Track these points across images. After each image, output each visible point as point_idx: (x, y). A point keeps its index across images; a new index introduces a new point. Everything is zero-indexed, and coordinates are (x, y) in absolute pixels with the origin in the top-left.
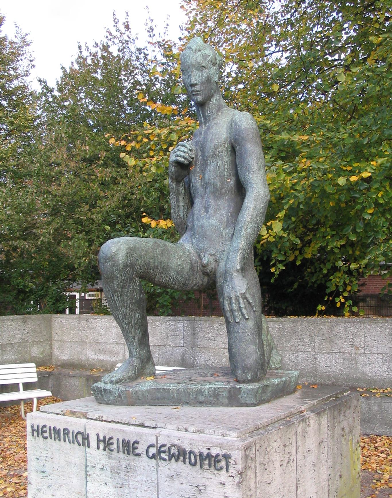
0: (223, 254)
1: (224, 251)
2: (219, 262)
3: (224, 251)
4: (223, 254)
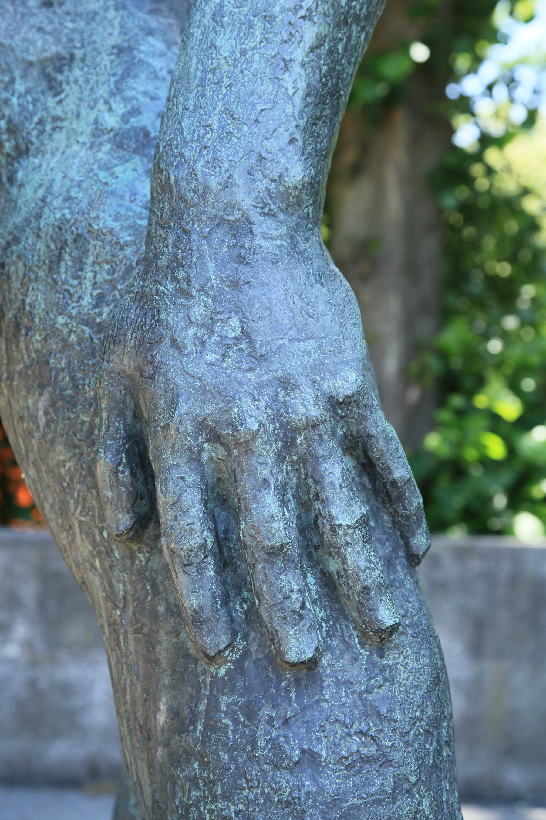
0: (54, 87)
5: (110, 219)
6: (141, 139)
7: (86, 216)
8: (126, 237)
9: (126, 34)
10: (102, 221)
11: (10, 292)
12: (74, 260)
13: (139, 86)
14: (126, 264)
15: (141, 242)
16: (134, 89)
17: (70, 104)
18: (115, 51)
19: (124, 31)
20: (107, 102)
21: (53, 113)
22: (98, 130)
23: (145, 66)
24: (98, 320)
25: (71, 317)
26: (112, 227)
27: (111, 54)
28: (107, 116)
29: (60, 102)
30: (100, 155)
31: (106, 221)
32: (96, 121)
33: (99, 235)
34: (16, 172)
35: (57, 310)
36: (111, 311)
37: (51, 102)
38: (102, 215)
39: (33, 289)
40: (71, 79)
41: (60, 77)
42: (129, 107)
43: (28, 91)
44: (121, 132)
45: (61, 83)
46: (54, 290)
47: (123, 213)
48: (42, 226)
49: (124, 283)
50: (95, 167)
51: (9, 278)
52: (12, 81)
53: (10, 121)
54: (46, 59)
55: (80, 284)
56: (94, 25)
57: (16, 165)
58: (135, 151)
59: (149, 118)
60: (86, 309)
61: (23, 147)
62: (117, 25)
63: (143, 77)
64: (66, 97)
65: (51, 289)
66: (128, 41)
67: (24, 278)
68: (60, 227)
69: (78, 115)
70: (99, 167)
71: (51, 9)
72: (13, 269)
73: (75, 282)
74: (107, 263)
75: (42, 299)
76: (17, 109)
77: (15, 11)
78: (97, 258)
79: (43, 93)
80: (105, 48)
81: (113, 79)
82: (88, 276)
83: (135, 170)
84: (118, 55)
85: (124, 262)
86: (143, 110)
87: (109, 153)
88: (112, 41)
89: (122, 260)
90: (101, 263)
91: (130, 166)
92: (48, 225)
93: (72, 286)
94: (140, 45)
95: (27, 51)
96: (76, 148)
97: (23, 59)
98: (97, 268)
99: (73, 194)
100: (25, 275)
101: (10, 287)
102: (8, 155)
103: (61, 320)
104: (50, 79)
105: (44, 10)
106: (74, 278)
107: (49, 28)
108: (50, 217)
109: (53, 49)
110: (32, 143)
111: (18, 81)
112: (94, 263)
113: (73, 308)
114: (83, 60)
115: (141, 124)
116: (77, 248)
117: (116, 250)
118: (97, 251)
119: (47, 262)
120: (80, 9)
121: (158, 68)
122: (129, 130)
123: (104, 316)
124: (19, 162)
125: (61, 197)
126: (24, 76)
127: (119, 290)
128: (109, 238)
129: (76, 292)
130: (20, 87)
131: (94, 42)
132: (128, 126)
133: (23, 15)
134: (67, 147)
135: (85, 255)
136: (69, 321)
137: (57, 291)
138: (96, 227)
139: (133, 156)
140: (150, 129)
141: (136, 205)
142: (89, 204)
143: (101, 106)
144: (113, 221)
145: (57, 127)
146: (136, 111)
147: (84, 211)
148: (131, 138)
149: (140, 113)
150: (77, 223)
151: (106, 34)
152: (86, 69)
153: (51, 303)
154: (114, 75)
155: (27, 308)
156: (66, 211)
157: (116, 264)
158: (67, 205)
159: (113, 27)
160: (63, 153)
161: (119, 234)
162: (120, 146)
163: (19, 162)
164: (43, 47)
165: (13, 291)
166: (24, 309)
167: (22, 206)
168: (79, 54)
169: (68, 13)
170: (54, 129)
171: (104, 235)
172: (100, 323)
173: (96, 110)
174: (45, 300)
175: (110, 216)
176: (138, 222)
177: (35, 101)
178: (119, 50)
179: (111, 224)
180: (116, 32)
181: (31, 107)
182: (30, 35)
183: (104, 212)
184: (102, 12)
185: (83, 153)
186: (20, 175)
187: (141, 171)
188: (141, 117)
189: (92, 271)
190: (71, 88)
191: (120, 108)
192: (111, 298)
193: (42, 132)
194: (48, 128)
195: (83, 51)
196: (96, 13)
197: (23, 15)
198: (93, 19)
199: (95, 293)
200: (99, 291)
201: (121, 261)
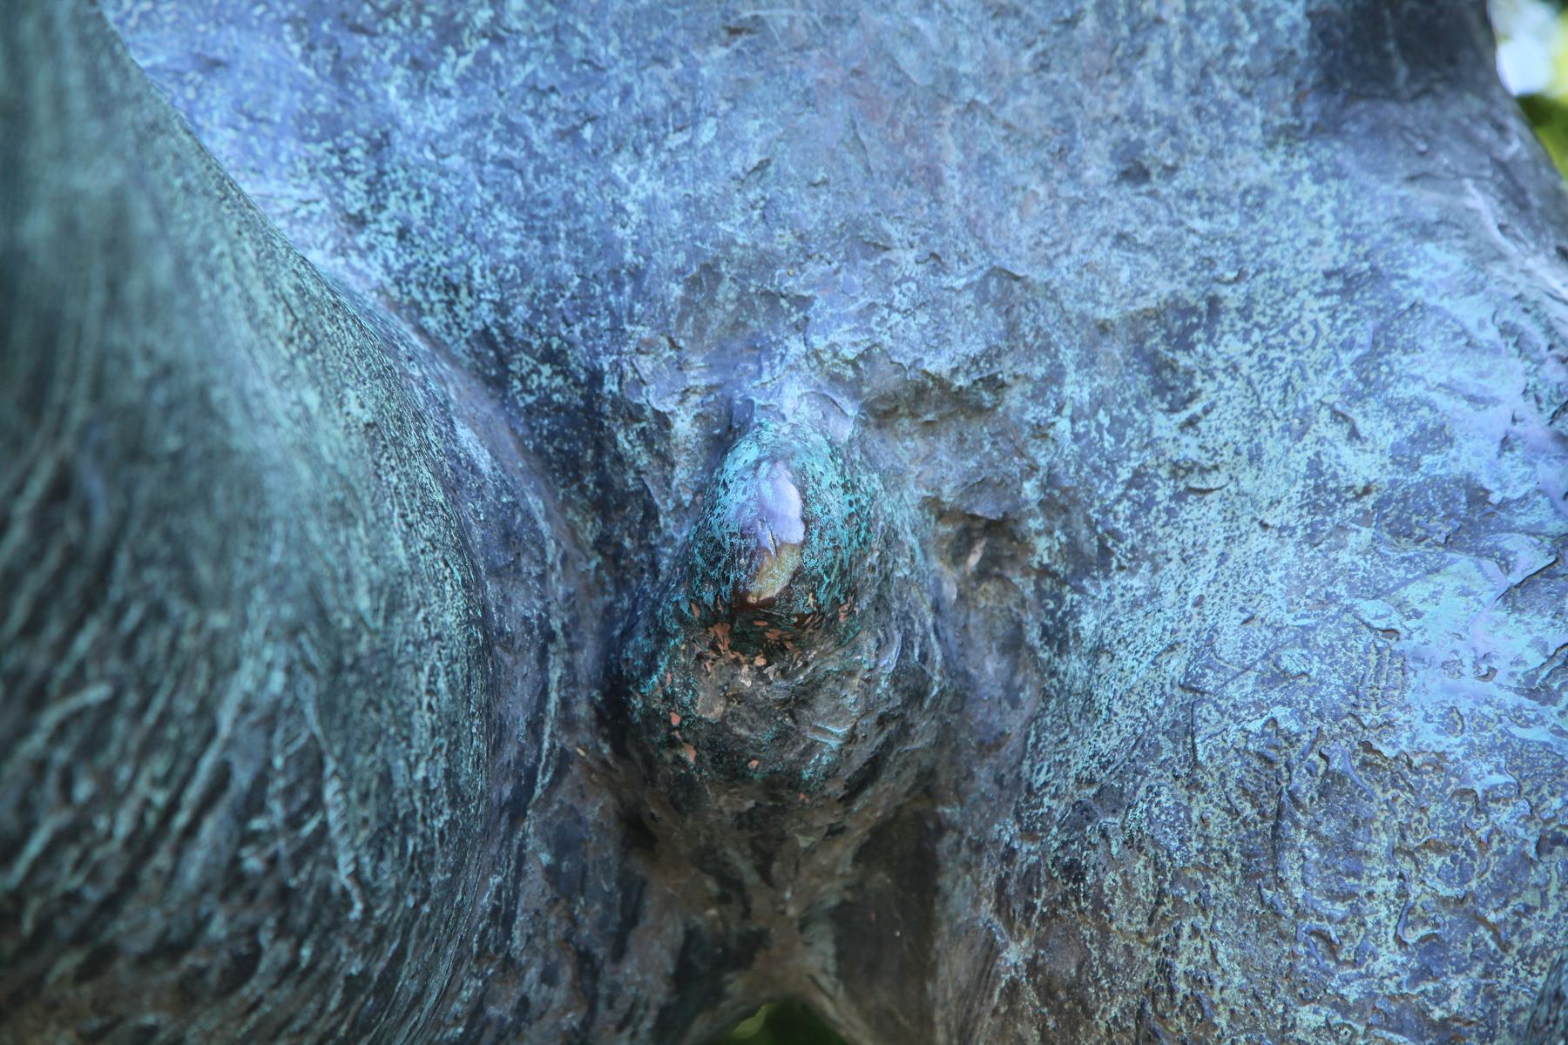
0: (1169, 386)
1: (1191, 320)
2: (1091, 560)
3: (1191, 320)
4: (1169, 386)
5: (1430, 727)
6: (1462, 509)
7: (1349, 721)
8: (1487, 776)
9: (1357, 240)
10: (1405, 735)
11: (1104, 947)
12: (1324, 845)
13: (1428, 369)
14: (1502, 852)
15: (1538, 789)
16: (1416, 379)
17: (1225, 426)
18: (1336, 284)
19: (1351, 233)
20: (1338, 417)
21: (1173, 453)
22: (1323, 493)
23: (1433, 320)
24: (1437, 1014)
25: (1341, 1005)
26: (1439, 749)
27: (1325, 293)
28: (1346, 452)
29: (1192, 422)
30: (1345, 557)
31: (1416, 731)
32: (1315, 467)
33: (1399, 772)
34: (1074, 614)
35: (1292, 988)
36: (1477, 988)
37: (1164, 425)
38: (1400, 717)
39: (1195, 931)
40: (1218, 363)
41: (1184, 360)
42: (1411, 427)
43: (1099, 402)
44: (1398, 494)
45: (1190, 374)
46: (1271, 933)
47: (1464, 710)
48: (1201, 757)
49: (1505, 904)
50: (1341, 588)
51: (1100, 905)
52: (1055, 376)
53: (1051, 480)
54: (1146, 315)
55: (1356, 911)
56: (1265, 221)
57: (1070, 597)
58: (1449, 543)
59: (1477, 454)
60: (1391, 985)
61: (1091, 547)
62: (1329, 220)
63: (1433, 345)
64: (1206, 411)
65: (1261, 929)
66: (1367, 257)
67: (1159, 903)
68: (1267, 761)
69: (1255, 457)
70: (1352, 588)
71: (1144, 188)
72: (1111, 878)
73: (1340, 909)
74: (1439, 850)
75: (1231, 959)
76: (1070, 448)
77: (1053, 194)
78: (1403, 837)
79: (1140, 404)
80: (1306, 279)
81: (1347, 358)
82: (1379, 890)
83: (1465, 593)
84: (1346, 293)
85: (1495, 845)
86: (1457, 432)
87: (1372, 549)
88: (1323, 260)
89: (1489, 841)
90: (1417, 849)
91: (1448, 582)
92: (1225, 752)
93: (1330, 918)
94: (1405, 266)
95: (1092, 295)
96: (1259, 542)
97: (1083, 317)
98: (1407, 866)
99: (1290, 660)
100: (1160, 894)
101: (1105, 931)
102: (1044, 571)
103: (1308, 1017)
104: (1157, 367)
105: (1126, 189)
106: (1333, 897)
107: (1146, 236)
108: (1222, 736)
109: (1163, 288)
110: (1118, 537)
111: (1071, 376)
112: (1394, 851)
113: (1346, 981)
114: (1245, 312)
115: (1456, 470)
116: (1330, 813)
117: (1463, 814)
118: (1402, 817)
119: (1235, 854)
120: (1223, 184)
121: (1471, 323)
122: (1420, 489)
123: (1456, 1003)
124: (1080, 590)
125: (1252, 674)
126: (1087, 362)
127: (1492, 927)
128: (1433, 780)
129: (1346, 934)
130: (1076, 389)
131: (1273, 266)
132: (1417, 478)
133: (1074, 205)
134: (1229, 540)
135: (1361, 833)
136: (1338, 1019)
137: (1282, 935)
138: (1388, 752)
139: (1449, 555)
140: (1485, 481)
141: (1500, 686)
142: (1350, 690)
143: (1324, 426)
144: (1438, 731)
145: (1190, 490)
146: (1437, 436)
147: (1338, 708)
148: (1431, 509)
149: (1450, 441)
150: (1320, 745)
151: (1301, 243)
152: (1256, 336)
153: (1265, 970)
154: (1349, 345)
155: (1182, 987)
156: (1279, 712)
157: (1469, 852)
158: (1275, 694)
159: (1319, 222)
160: (1223, 558)
161: (1466, 769)
162: (1401, 531)
163: (1080, 590)
164: (1134, 284)
165: (1117, 942)
166: (1172, 991)
167: (1117, 706)
168: (1232, 297)
169: (1191, 195)
170: (1179, 497)
171: (1417, 771)
172: (1443, 1020)
173: (1307, 439)
174: (1245, 964)
175: (1427, 718)
176: (1517, 731)
177: (1119, 427)
178: (1347, 282)
179: (1431, 738)
180: (1330, 237)
181: (1109, 440)
182: (1098, 255)
183: (1407, 708)
184: (1281, 189)
185: (1288, 554)
186: (1088, 623)
187: (1487, 596)
188: (1453, 452)
189: (1390, 875)
190: (1221, 386)
191: (1382, 431)
192: (1469, 949)
193: (1147, 505)
194: (1163, 494)
195: (1242, 289)
196: (1265, 191)
197: (1074, 205)
198: (1260, 205)
199: (1411, 937)
200: (1423, 931)
201: (1484, 845)
